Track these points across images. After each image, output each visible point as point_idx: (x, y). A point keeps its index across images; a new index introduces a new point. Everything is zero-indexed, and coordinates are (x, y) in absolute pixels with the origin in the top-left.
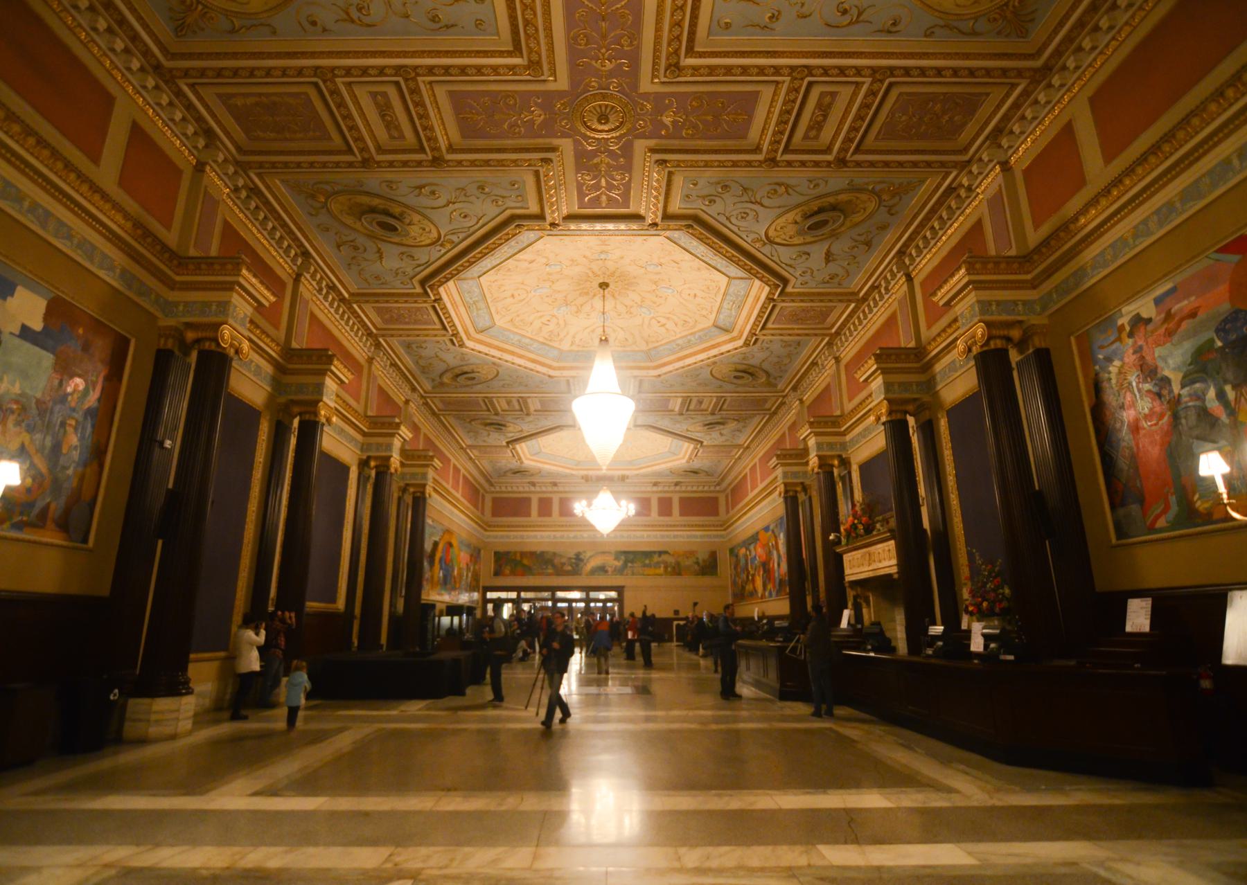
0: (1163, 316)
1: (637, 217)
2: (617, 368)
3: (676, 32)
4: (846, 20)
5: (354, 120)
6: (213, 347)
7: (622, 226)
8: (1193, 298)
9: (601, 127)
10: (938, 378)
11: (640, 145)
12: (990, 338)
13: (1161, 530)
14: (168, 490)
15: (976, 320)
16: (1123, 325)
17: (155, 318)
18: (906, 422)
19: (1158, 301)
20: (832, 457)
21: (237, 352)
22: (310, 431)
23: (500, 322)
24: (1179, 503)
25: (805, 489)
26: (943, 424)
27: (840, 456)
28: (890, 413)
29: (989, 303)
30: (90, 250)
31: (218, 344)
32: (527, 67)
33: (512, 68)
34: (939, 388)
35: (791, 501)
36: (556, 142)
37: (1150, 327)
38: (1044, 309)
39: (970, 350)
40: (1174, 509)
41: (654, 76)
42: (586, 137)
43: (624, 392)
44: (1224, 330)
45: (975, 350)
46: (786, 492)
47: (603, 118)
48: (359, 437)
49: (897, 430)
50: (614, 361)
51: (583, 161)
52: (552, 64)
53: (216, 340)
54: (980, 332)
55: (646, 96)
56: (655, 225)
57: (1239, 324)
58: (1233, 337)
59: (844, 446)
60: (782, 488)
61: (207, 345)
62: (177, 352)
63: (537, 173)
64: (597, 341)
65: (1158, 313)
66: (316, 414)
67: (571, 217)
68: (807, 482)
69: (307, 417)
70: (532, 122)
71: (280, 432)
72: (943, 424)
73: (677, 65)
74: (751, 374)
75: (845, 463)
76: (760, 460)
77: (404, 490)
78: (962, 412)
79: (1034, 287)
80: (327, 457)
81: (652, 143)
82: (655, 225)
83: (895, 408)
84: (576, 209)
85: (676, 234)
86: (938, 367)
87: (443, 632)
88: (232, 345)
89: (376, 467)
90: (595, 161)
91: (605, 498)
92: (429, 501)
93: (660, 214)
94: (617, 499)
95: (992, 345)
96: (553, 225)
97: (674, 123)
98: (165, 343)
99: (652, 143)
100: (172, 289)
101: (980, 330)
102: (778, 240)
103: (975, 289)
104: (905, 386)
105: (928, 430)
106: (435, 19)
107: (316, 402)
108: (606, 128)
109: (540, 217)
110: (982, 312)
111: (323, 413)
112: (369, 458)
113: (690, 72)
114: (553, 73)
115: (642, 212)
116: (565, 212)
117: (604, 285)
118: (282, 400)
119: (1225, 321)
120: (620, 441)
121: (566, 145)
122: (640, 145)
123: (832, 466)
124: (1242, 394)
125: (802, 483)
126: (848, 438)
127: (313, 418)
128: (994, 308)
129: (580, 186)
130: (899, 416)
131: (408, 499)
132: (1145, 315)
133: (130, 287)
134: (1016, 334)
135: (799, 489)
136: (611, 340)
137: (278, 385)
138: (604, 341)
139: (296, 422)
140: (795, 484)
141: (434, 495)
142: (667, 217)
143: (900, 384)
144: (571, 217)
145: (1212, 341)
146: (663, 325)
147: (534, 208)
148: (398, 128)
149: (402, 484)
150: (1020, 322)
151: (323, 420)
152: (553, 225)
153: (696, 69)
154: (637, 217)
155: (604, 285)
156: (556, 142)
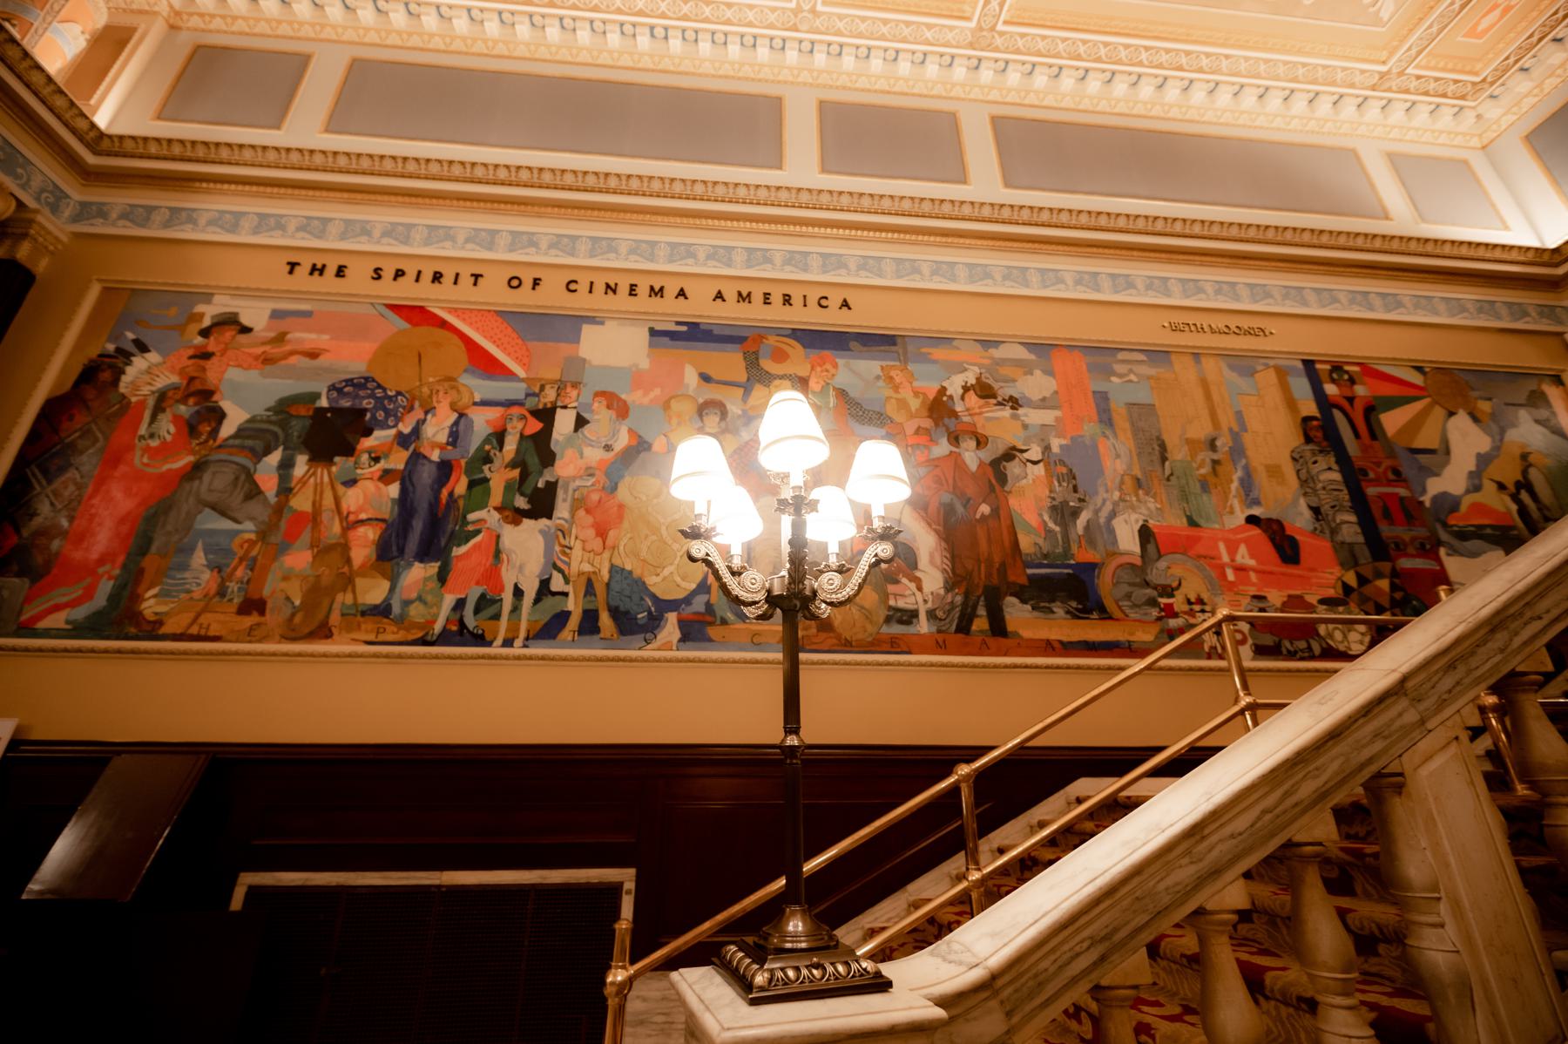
0: (272, 334)
5: (91, 204)
8: (326, 337)
13: (47, 633)
14: (536, 488)
16: (202, 315)
19: (276, 315)
24: (114, 598)
37: (243, 338)
40: (100, 600)
44: (340, 391)
57: (361, 393)
58: (346, 403)
65: (267, 329)
87: (349, 437)
119: (349, 382)
124: (314, 474)
127: (1528, 861)
132: (245, 320)
145: (317, 396)
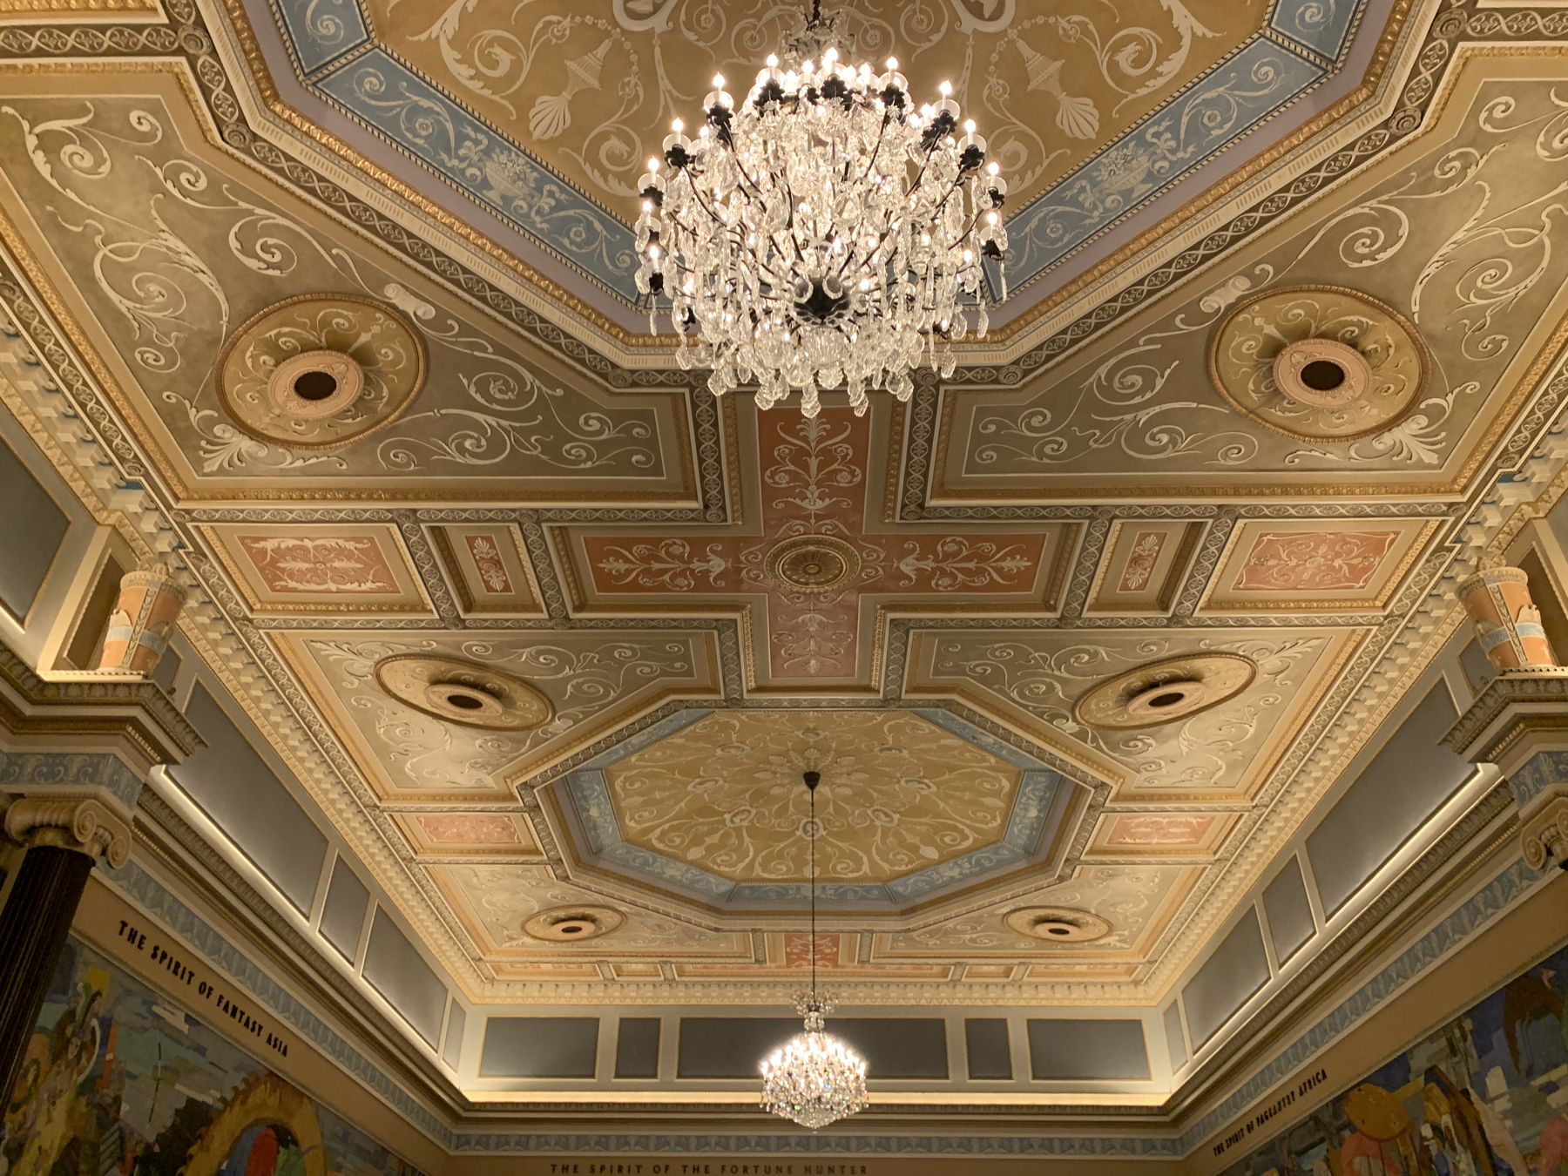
39: (1550, 853)
61: (50, 838)
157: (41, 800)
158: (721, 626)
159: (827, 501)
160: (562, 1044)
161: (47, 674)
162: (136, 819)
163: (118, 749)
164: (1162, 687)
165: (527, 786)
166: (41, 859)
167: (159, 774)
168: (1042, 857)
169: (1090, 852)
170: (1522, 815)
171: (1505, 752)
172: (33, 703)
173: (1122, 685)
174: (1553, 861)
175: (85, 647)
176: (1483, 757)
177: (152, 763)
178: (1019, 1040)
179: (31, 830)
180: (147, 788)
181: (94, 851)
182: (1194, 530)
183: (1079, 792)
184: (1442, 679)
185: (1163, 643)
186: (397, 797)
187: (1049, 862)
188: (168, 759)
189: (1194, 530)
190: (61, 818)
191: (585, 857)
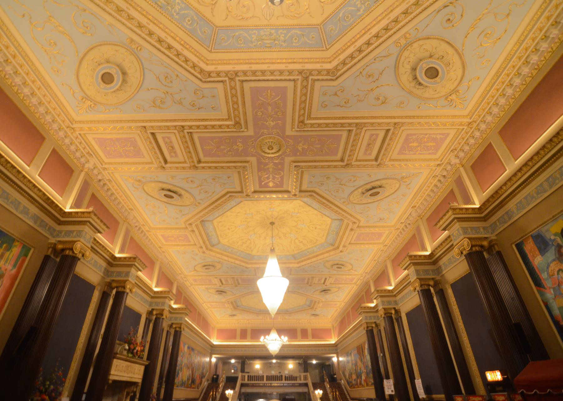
1: (288, 192)
2: (279, 263)
3: (304, 91)
4: (380, 102)
6: (71, 253)
7: (280, 196)
9: (269, 151)
10: (443, 267)
11: (288, 160)
12: (472, 246)
15: (462, 237)
17: (48, 238)
18: (430, 290)
20: (391, 309)
21: (83, 256)
22: (120, 296)
23: (224, 241)
25: (377, 325)
26: (450, 292)
27: (394, 308)
28: (421, 286)
29: (467, 228)
30: (17, 204)
31: (73, 252)
32: (234, 125)
33: (228, 126)
34: (444, 273)
35: (370, 333)
36: (248, 159)
38: (493, 231)
39: (462, 253)
41: (292, 128)
42: (263, 157)
43: (283, 276)
45: (465, 253)
46: (368, 327)
47: (271, 148)
48: (149, 299)
49: (426, 294)
50: (278, 260)
51: (261, 167)
52: (246, 122)
53: (72, 249)
54: (466, 243)
55: (289, 137)
56: (295, 195)
59: (396, 302)
60: (365, 326)
61: (178, 329)
62: (52, 256)
63: (239, 172)
64: (269, 250)
66: (124, 287)
67: (255, 192)
68: (378, 322)
69: (120, 289)
70: (238, 149)
71: (104, 296)
72: (450, 292)
73: (302, 122)
74: (213, 266)
75: (397, 312)
76: (352, 309)
77: (171, 326)
78: (461, 286)
79: (485, 221)
80: (128, 309)
81: (293, 158)
82: (295, 195)
83: (423, 283)
84: (258, 189)
85: (305, 199)
86: (441, 262)
88: (80, 252)
89: (156, 315)
90: (267, 167)
91: (274, 335)
92: (183, 332)
93: (298, 190)
94: (280, 336)
95: (474, 249)
96: (247, 195)
97: (303, 149)
98: (69, 253)
99: (293, 158)
100: (59, 224)
101: (466, 242)
102: (355, 202)
103: (458, 221)
104: (426, 272)
105: (441, 294)
106: (193, 105)
107: (125, 281)
108: (273, 151)
109: (241, 192)
110: (465, 233)
111: (128, 287)
112: (153, 310)
113: (310, 126)
114: (247, 127)
115: (290, 190)
116: (253, 190)
117: (272, 224)
118: (108, 280)
120: (281, 301)
121: (253, 160)
122: (288, 160)
123: (391, 313)
125: (375, 322)
126: (398, 297)
128: (469, 230)
129: (260, 178)
130: (426, 287)
131: (172, 331)
133: (35, 223)
134: (485, 243)
135: (374, 325)
136: (276, 250)
137: (107, 273)
138: (272, 250)
139: (114, 292)
140: (372, 323)
141: (186, 329)
142: (301, 191)
143: (472, 228)
144: (255, 192)
146: (302, 242)
147: (239, 189)
148: (166, 143)
149: (170, 323)
150: (486, 238)
151: (128, 291)
152: (247, 195)
153: (312, 125)
154: (288, 192)
155: (272, 224)
156: (248, 159)
157: (176, 324)
158: (244, 167)
159: (275, 123)
160: (231, 334)
161: (117, 255)
162: (135, 283)
163: (87, 229)
164: (373, 191)
165: (190, 224)
166: (65, 258)
167: (139, 273)
168: (336, 245)
169: (357, 160)
170: (454, 244)
171: (451, 228)
172: (63, 217)
173: (360, 190)
174: (463, 255)
175: (77, 204)
176: (405, 269)
177: (95, 233)
178: (310, 332)
179: (175, 328)
180: (95, 239)
181: (80, 256)
182: (326, 279)
183: (315, 302)
184: (490, 143)
185: (376, 174)
186: (80, 122)
187: (313, 308)
188: (140, 271)
189: (326, 279)
190: (71, 247)
191: (209, 246)
